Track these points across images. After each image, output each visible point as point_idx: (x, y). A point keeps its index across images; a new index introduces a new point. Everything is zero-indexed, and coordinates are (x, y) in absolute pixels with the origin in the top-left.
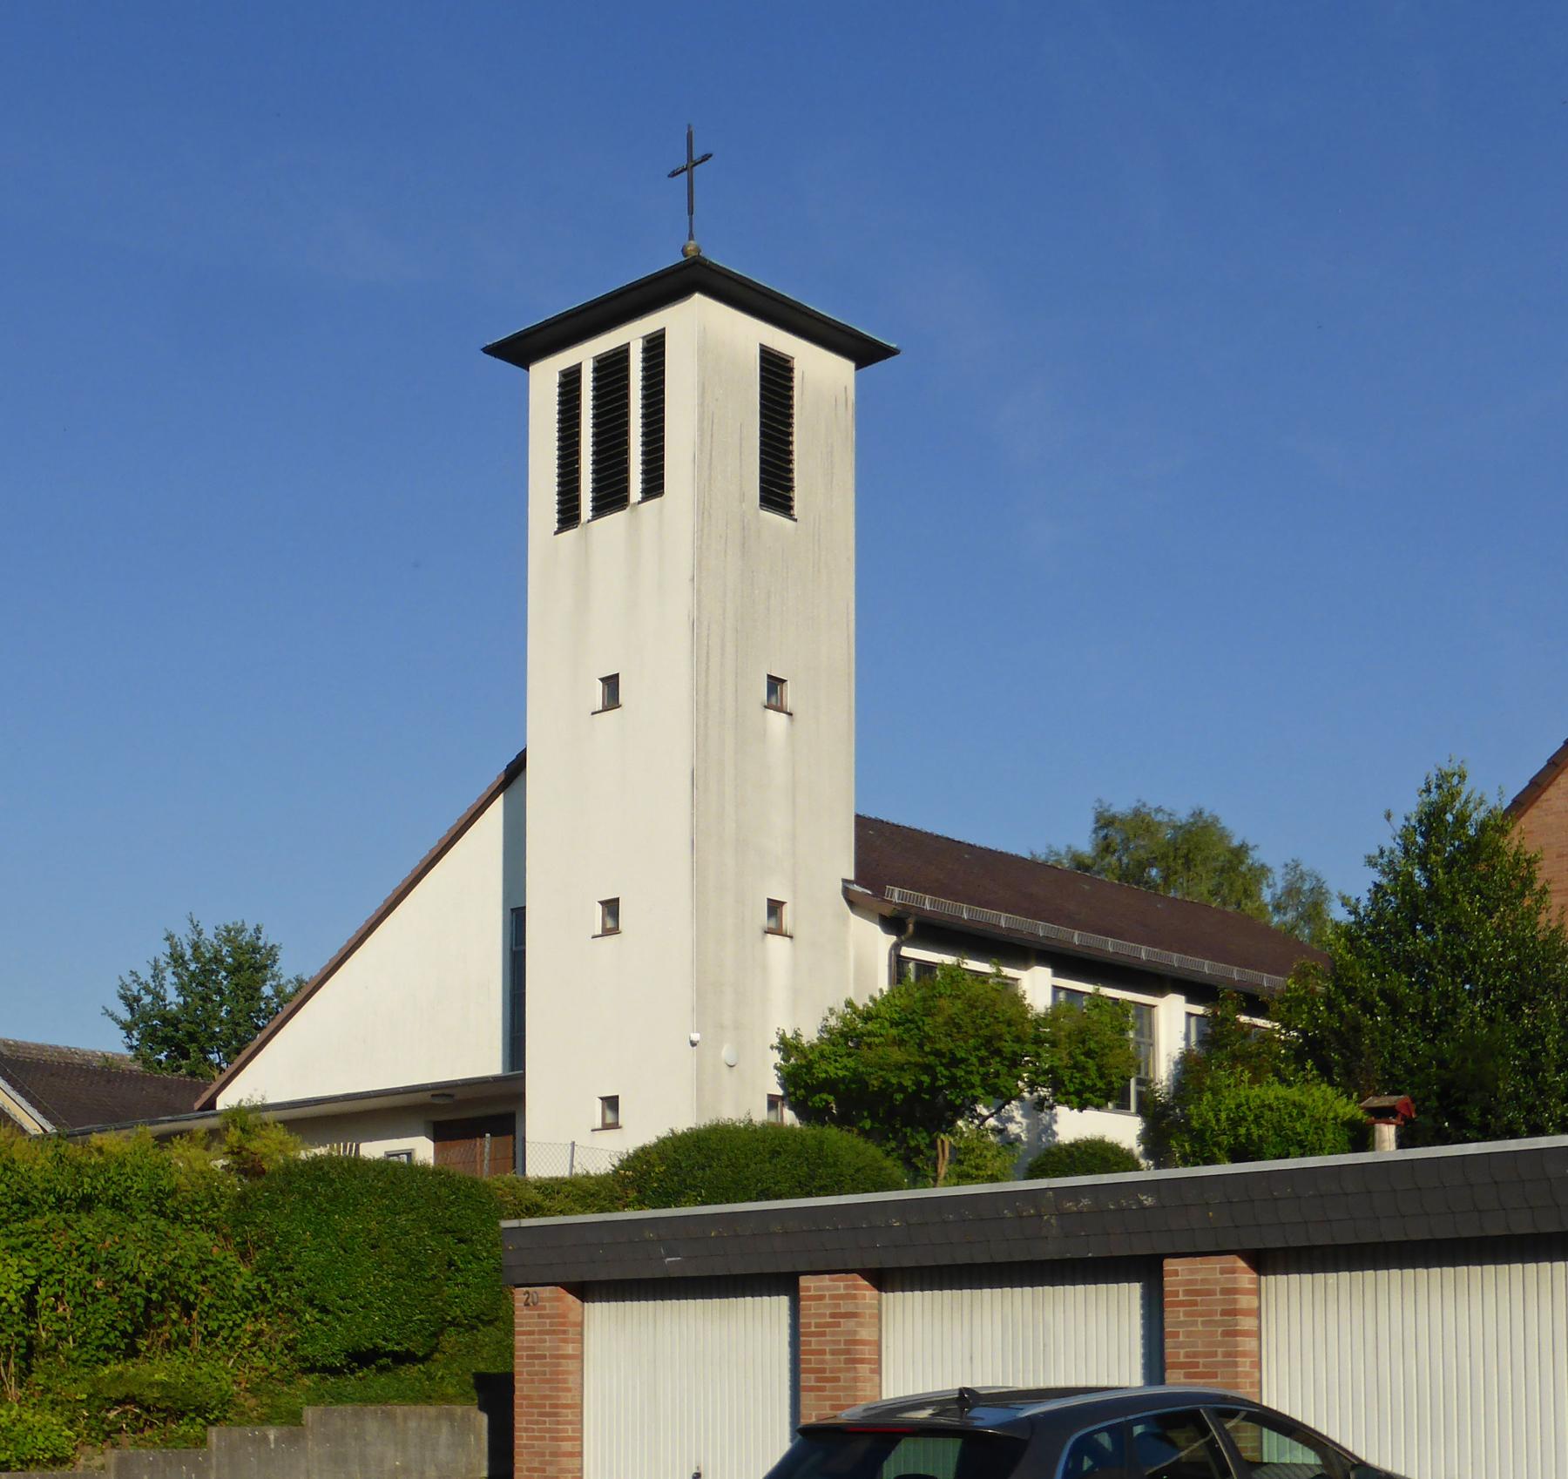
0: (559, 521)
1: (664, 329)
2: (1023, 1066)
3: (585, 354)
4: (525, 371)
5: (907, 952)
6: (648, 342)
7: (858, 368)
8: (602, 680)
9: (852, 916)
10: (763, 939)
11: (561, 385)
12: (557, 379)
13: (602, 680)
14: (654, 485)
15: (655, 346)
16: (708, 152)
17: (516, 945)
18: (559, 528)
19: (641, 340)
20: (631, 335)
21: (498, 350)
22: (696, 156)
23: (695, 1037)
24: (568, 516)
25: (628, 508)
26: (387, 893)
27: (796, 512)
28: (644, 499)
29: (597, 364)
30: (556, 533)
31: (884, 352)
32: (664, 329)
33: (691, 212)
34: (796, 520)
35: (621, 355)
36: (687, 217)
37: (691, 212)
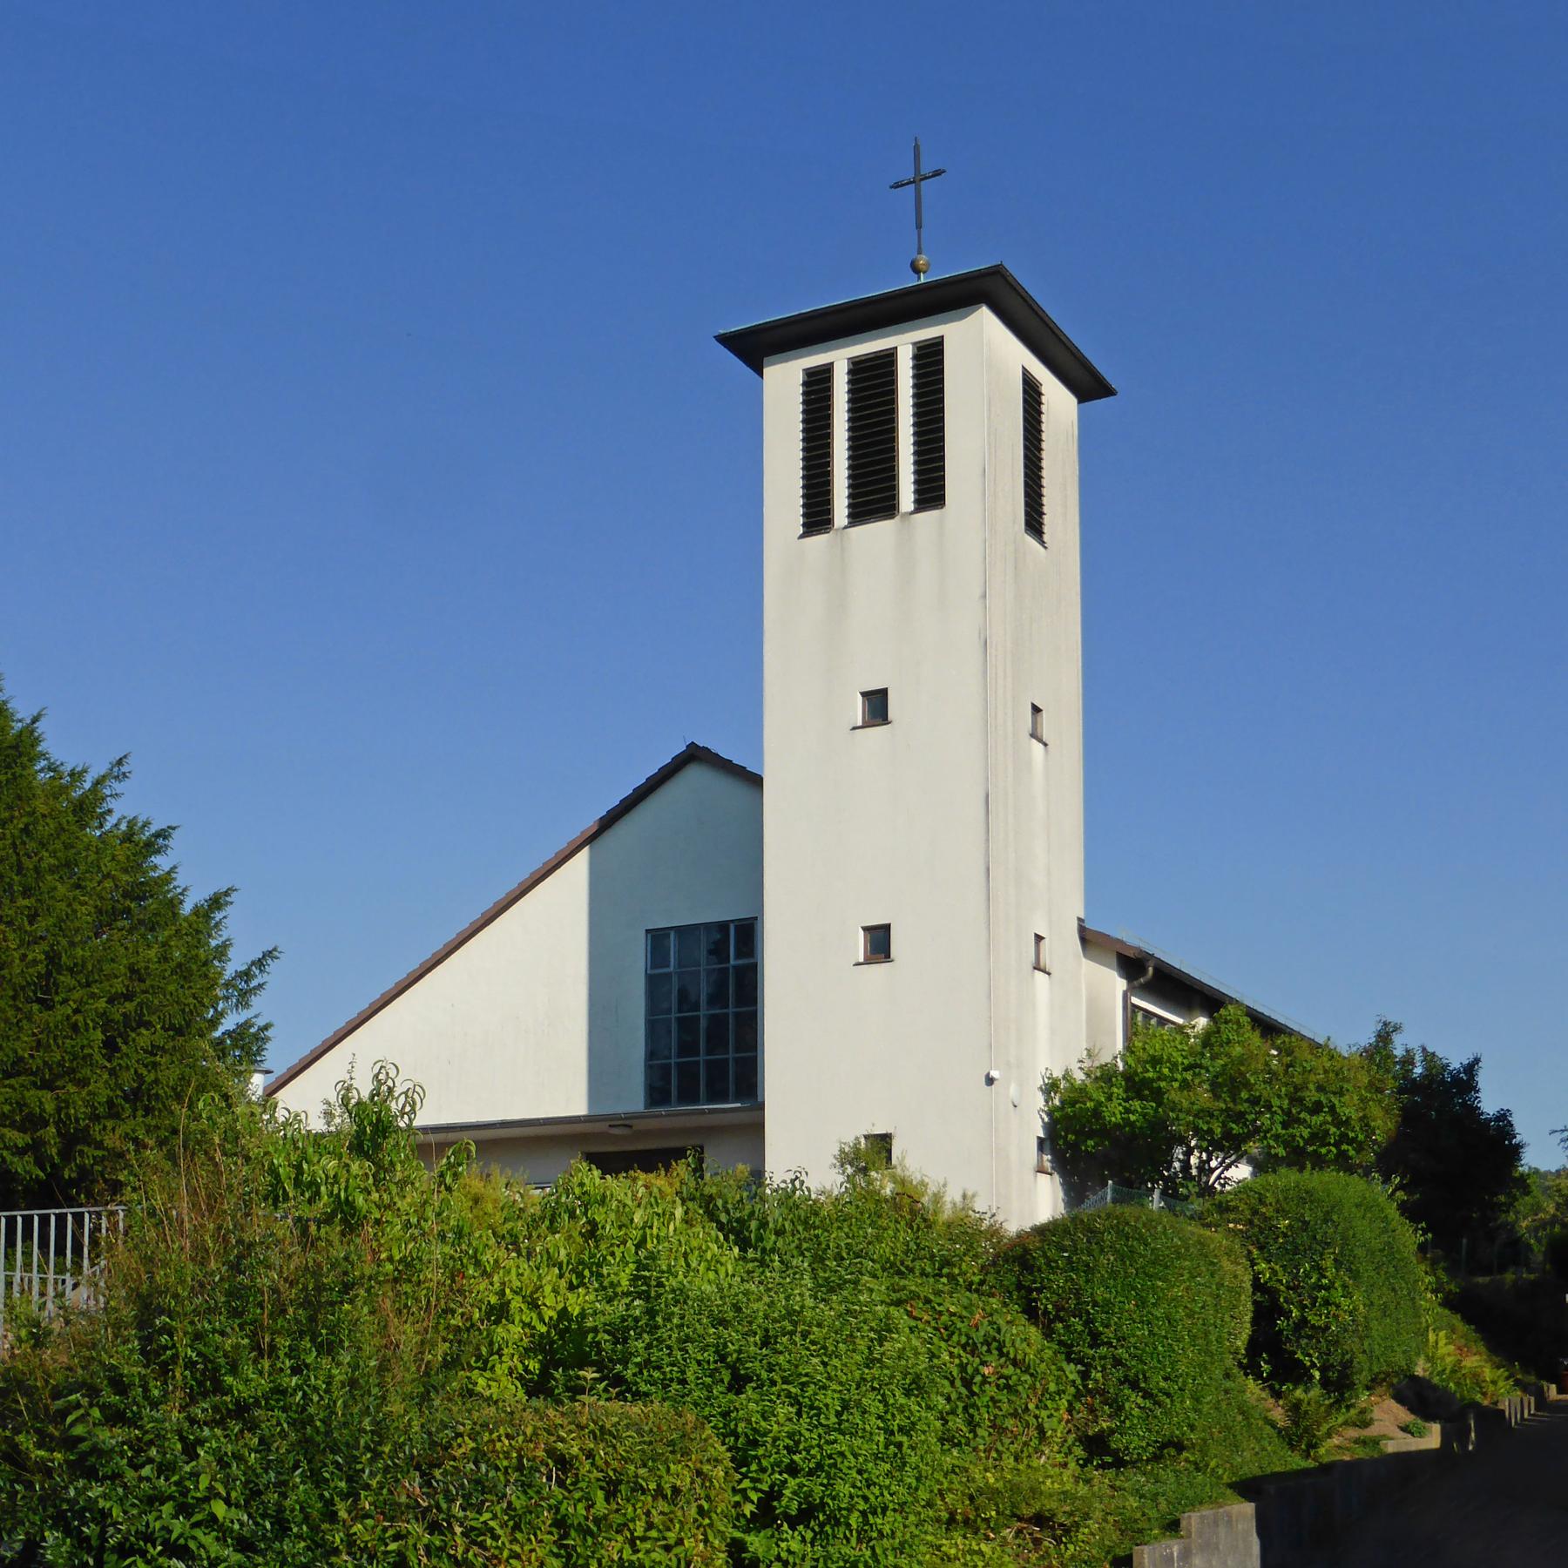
0: (849, 516)
1: (943, 337)
2: (123, 1120)
3: (840, 358)
4: (749, 372)
5: (1135, 1001)
6: (919, 349)
7: (1080, 402)
8: (864, 694)
9: (1084, 960)
10: (1033, 973)
11: (805, 384)
12: (800, 378)
13: (864, 694)
14: (931, 493)
15: (930, 359)
16: (942, 168)
17: (651, 968)
18: (804, 533)
19: (911, 346)
20: (903, 344)
21: (728, 341)
22: (926, 169)
23: (994, 1074)
24: (817, 518)
25: (897, 518)
26: (487, 905)
27: (1046, 538)
28: (917, 511)
29: (851, 366)
30: (801, 537)
31: (1105, 391)
32: (943, 337)
33: (919, 226)
34: (1046, 548)
35: (889, 358)
36: (916, 232)
37: (919, 226)
